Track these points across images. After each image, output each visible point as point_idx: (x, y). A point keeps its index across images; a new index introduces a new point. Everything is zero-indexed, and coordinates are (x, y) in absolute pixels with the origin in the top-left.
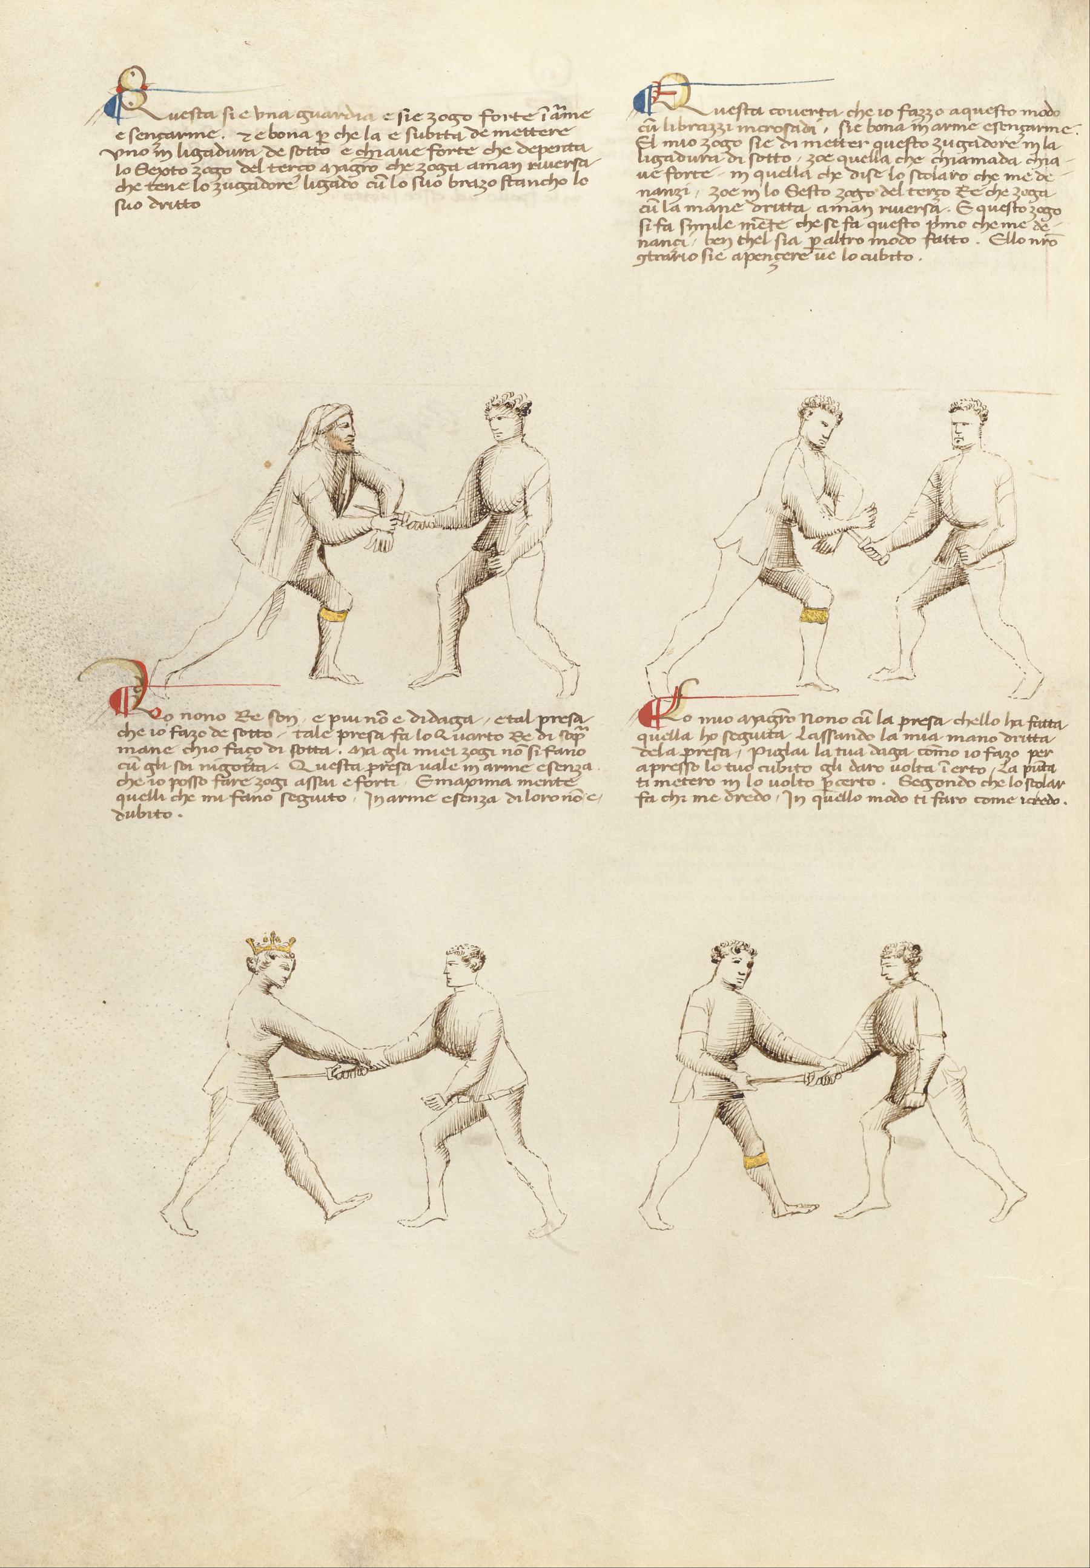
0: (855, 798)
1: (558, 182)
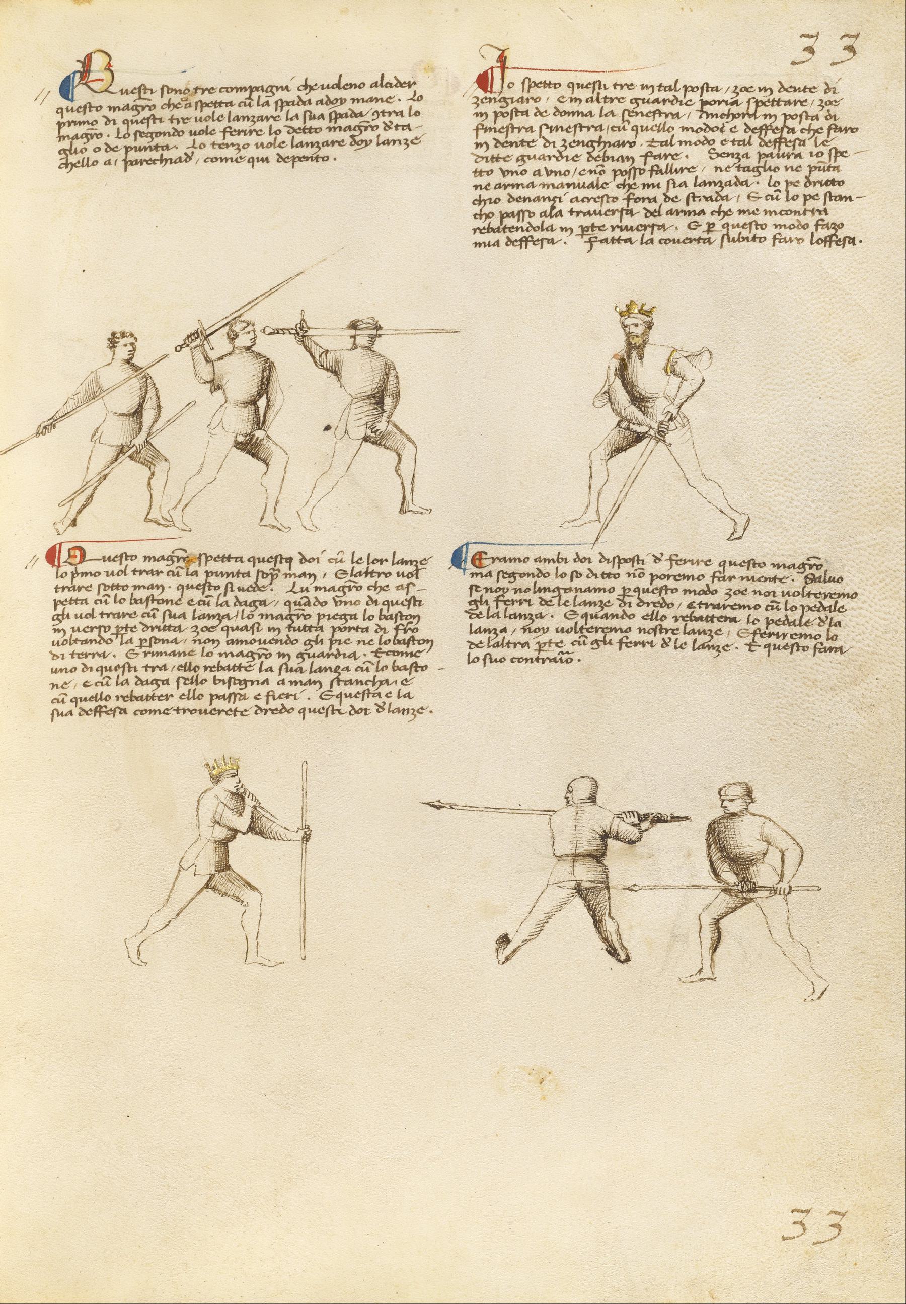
0: (385, 642)
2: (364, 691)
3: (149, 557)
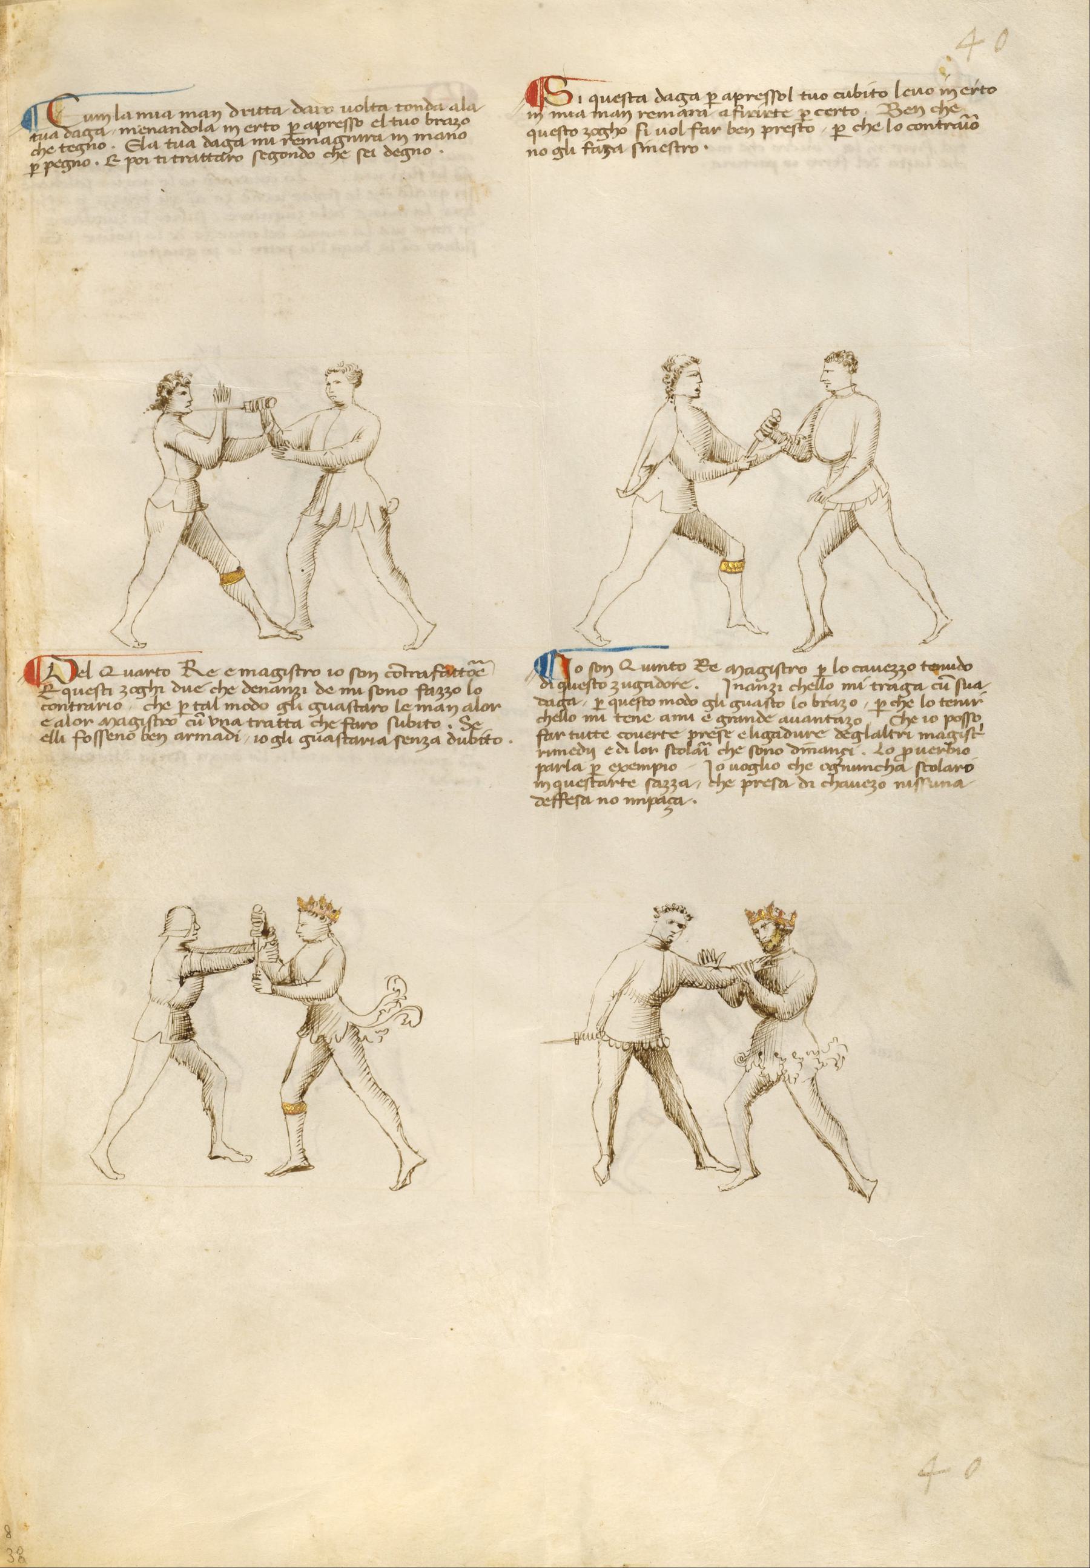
1: (872, 128)
2: (350, 704)
3: (247, 670)
